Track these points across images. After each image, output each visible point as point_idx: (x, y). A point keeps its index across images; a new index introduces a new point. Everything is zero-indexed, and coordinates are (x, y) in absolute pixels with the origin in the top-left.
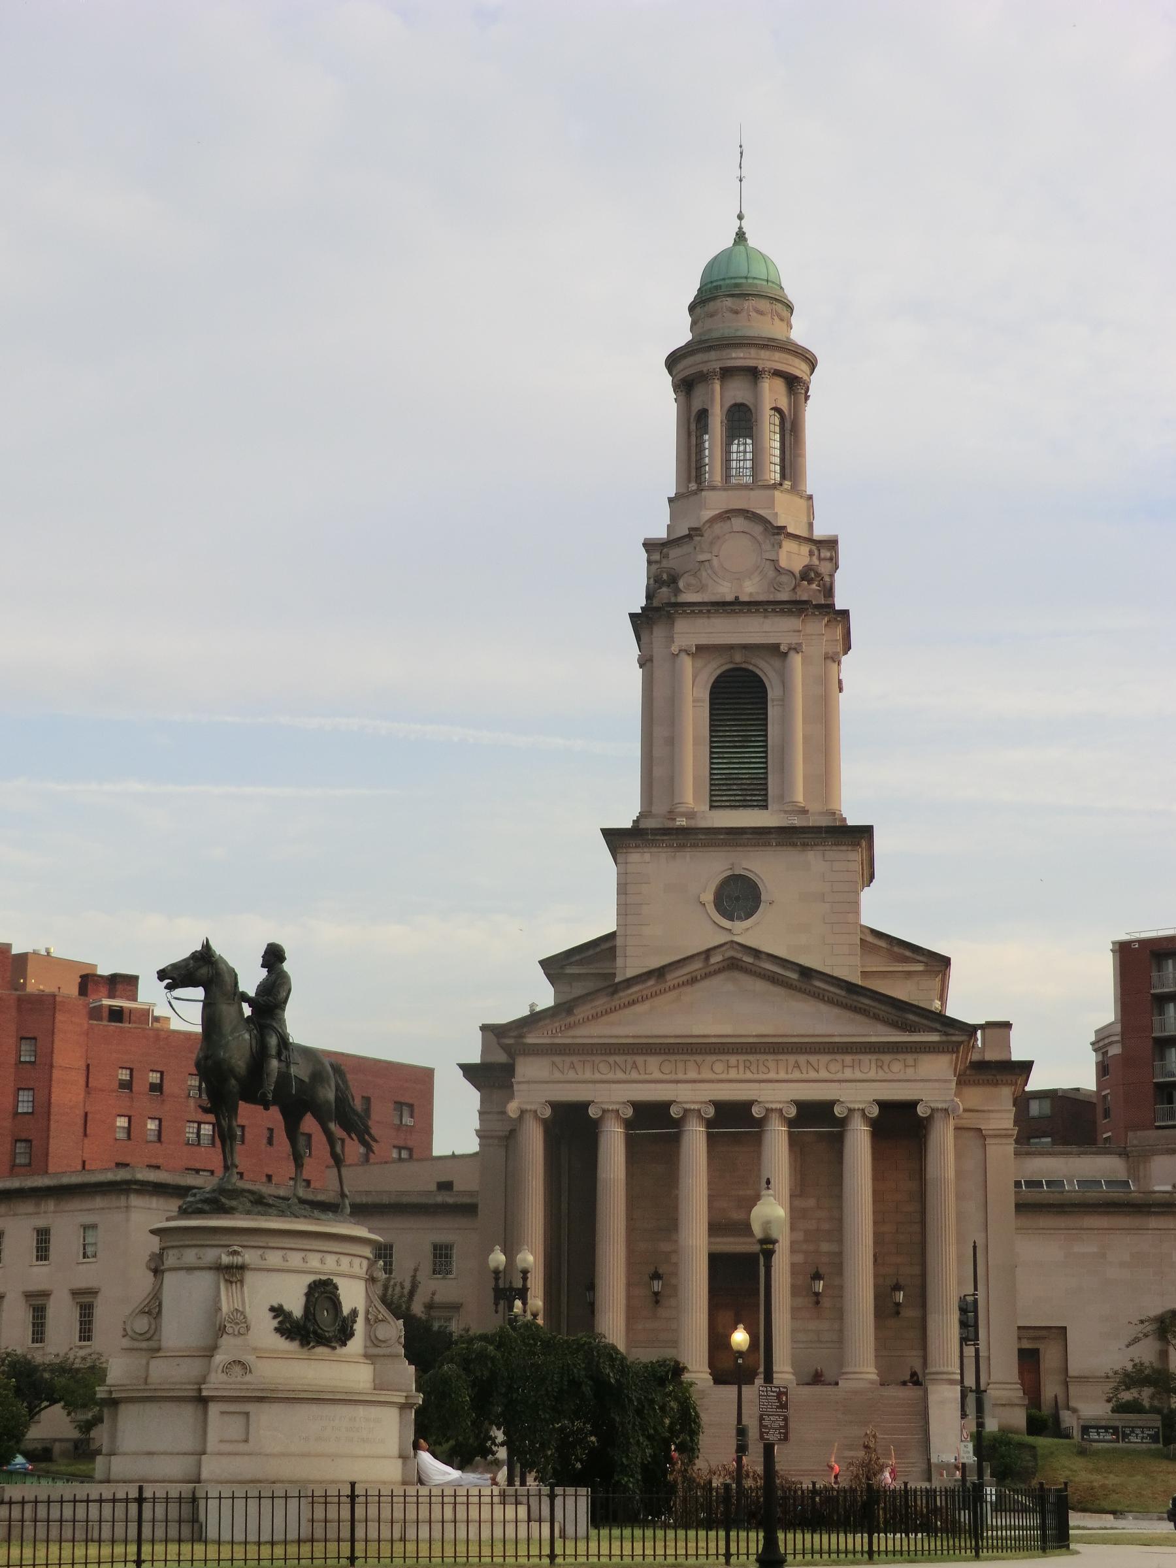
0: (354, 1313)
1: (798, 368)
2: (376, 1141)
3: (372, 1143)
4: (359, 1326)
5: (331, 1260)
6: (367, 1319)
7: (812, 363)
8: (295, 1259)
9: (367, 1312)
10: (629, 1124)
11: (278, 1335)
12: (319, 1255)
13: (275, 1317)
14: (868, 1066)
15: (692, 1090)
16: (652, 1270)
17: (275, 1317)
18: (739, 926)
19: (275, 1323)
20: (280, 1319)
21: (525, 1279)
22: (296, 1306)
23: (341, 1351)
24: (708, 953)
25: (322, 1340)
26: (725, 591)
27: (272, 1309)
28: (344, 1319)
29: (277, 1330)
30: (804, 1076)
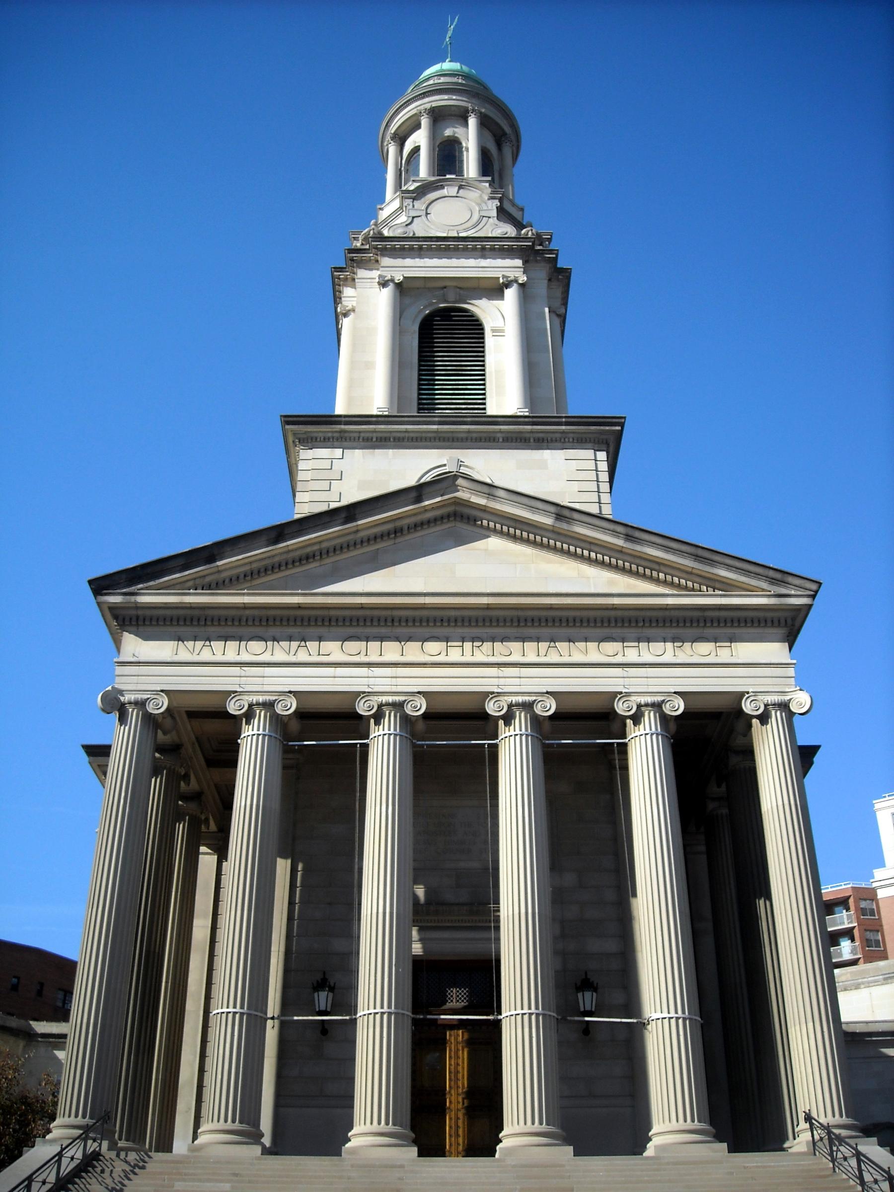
16: (319, 976)
24: (418, 492)
30: (566, 659)
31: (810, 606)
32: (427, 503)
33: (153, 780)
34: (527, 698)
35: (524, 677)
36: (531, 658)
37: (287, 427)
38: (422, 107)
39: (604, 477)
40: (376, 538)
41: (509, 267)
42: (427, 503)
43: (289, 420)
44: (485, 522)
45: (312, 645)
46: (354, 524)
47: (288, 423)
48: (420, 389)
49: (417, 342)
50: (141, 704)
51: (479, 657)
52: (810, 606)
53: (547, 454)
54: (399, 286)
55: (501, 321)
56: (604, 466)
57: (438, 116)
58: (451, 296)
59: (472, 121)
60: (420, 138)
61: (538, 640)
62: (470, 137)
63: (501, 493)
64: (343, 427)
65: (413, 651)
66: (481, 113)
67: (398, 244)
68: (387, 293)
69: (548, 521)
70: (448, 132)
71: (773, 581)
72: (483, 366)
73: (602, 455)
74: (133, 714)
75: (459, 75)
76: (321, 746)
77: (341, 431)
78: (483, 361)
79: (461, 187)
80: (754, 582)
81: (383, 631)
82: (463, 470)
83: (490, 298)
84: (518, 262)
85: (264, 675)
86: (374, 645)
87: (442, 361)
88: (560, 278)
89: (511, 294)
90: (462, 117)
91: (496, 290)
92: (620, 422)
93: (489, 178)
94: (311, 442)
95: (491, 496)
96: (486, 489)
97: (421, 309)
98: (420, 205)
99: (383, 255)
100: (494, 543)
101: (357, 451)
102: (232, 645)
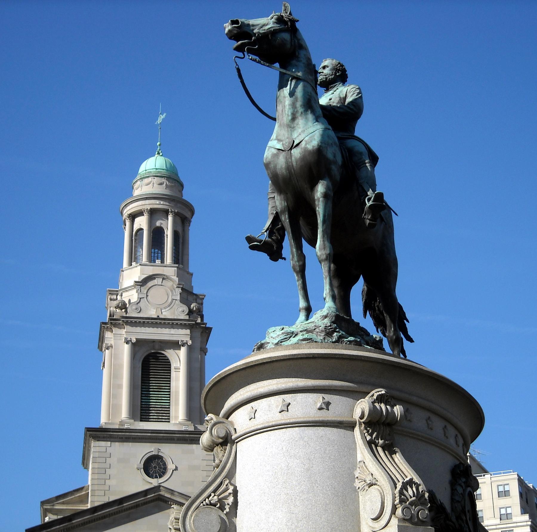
1: (187, 214)
2: (410, 340)
7: (193, 213)
18: (155, 482)
24: (146, 493)
26: (152, 313)
31: (361, 96)
32: (149, 496)
37: (88, 433)
41: (182, 335)
42: (149, 496)
43: (88, 430)
44: (170, 503)
46: (122, 506)
47: (88, 431)
48: (142, 399)
49: (140, 374)
52: (361, 96)
55: (179, 360)
57: (153, 213)
58: (157, 347)
59: (170, 218)
60: (142, 222)
62: (168, 225)
63: (176, 493)
64: (111, 433)
66: (175, 212)
67: (134, 320)
68: (126, 348)
70: (158, 224)
72: (170, 386)
75: (164, 177)
77: (110, 435)
78: (170, 384)
79: (163, 279)
83: (174, 349)
84: (188, 331)
87: (153, 384)
89: (183, 350)
90: (166, 213)
91: (176, 345)
93: (177, 265)
94: (98, 438)
96: (171, 492)
97: (142, 353)
98: (144, 289)
99: (127, 325)
101: (117, 443)
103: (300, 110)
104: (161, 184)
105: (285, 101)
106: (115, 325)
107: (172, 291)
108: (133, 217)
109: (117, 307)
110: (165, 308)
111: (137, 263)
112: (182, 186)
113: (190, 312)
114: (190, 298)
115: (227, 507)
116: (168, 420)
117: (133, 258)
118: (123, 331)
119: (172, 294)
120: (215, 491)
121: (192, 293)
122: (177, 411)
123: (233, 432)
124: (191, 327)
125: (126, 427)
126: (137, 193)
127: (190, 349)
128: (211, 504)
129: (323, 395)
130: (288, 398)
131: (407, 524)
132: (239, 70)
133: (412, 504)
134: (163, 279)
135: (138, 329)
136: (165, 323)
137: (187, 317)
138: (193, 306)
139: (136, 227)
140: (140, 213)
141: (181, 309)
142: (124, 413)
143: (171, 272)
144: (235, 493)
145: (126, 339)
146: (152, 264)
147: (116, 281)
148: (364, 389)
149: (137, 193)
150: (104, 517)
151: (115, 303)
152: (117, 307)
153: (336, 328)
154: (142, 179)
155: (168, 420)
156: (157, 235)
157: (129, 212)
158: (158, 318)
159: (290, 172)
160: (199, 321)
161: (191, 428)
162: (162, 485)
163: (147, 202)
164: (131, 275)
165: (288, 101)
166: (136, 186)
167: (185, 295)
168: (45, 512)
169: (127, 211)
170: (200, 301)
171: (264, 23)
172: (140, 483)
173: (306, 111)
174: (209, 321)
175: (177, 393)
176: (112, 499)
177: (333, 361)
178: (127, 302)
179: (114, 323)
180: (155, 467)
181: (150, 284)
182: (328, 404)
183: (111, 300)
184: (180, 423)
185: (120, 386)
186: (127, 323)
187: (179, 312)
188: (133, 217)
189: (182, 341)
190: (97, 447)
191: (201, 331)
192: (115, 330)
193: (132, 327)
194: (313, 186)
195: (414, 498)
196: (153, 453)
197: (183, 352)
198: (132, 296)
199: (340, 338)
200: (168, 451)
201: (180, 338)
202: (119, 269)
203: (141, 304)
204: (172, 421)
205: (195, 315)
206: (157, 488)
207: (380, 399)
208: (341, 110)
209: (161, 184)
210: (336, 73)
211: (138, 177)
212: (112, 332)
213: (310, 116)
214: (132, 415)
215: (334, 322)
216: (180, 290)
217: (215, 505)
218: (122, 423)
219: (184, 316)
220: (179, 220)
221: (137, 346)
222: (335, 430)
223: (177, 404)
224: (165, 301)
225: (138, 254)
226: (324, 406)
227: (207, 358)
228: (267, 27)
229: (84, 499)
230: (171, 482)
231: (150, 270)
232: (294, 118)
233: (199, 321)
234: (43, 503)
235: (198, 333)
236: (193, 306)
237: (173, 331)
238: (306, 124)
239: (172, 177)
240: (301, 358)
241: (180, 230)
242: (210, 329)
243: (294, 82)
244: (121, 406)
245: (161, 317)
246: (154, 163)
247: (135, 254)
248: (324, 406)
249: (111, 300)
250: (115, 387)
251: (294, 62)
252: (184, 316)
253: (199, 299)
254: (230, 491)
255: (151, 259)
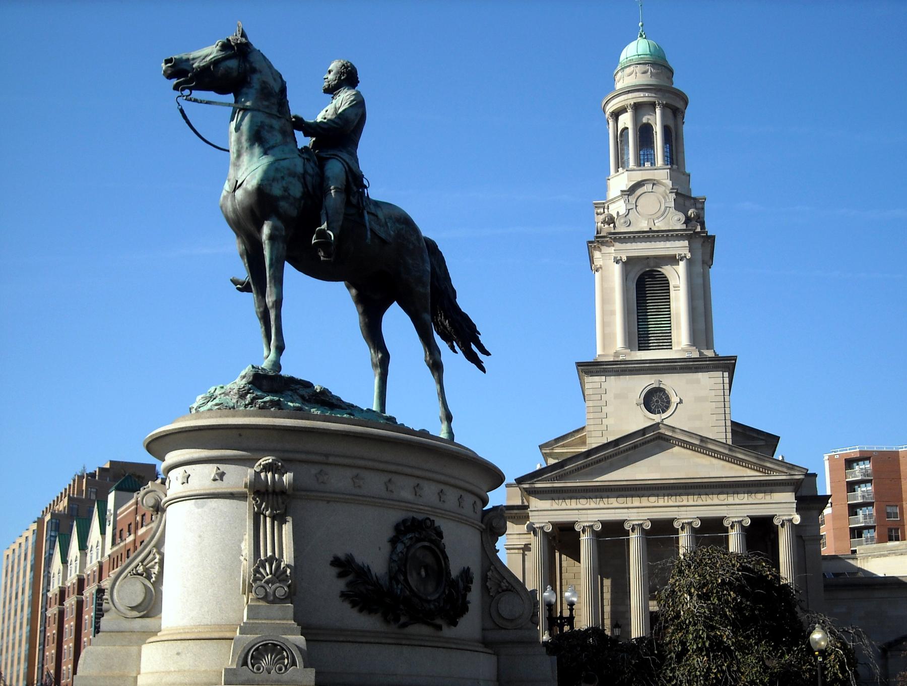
0: (466, 574)
1: (680, 105)
2: (488, 354)
3: (481, 356)
4: (474, 597)
5: (430, 492)
6: (485, 589)
7: (686, 102)
8: (374, 484)
9: (485, 578)
10: (694, 531)
11: (347, 605)
12: (413, 482)
13: (340, 575)
14: (743, 498)
15: (637, 513)
17: (340, 575)
18: (657, 418)
19: (341, 585)
20: (350, 578)
21: (571, 610)
22: (375, 558)
23: (448, 632)
24: (644, 431)
25: (425, 616)
26: (644, 225)
27: (336, 562)
28: (453, 584)
29: (343, 595)
31: (359, 104)
33: (474, 347)
34: (690, 520)
35: (687, 511)
36: (691, 503)
38: (628, 102)
39: (727, 386)
40: (627, 450)
41: (680, 247)
43: (579, 364)
45: (605, 500)
50: (541, 528)
51: (671, 503)
53: (700, 375)
54: (625, 264)
55: (677, 278)
56: (727, 380)
57: (637, 108)
58: (652, 263)
59: (658, 111)
60: (626, 120)
61: (694, 495)
62: (657, 121)
65: (645, 501)
69: (697, 442)
70: (645, 120)
71: (788, 468)
73: (726, 374)
74: (539, 532)
76: (612, 535)
79: (654, 184)
80: (781, 469)
81: (633, 493)
82: (661, 386)
84: (686, 243)
85: (588, 514)
86: (629, 499)
87: (651, 306)
88: (710, 241)
90: (653, 105)
91: (673, 260)
92: (735, 358)
95: (673, 431)
98: (632, 199)
100: (677, 449)
102: (573, 501)
103: (245, 144)
104: (645, 72)
105: (233, 134)
106: (603, 243)
107: (664, 198)
108: (616, 115)
109: (604, 222)
110: (658, 218)
111: (623, 168)
112: (671, 71)
113: (688, 220)
114: (688, 203)
115: (153, 576)
116: (670, 347)
117: (620, 163)
118: (612, 250)
119: (665, 200)
120: (142, 562)
121: (689, 198)
122: (679, 335)
123: (163, 496)
124: (689, 238)
125: (621, 358)
126: (619, 86)
127: (690, 263)
128: (139, 574)
129: (218, 465)
130: (187, 468)
131: (262, 603)
132: (182, 111)
133: (267, 582)
134: (654, 184)
135: (628, 246)
136: (658, 236)
137: (684, 227)
138: (691, 212)
139: (620, 128)
140: (623, 110)
141: (676, 218)
142: (619, 342)
143: (663, 175)
144: (161, 563)
145: (615, 258)
146: (642, 168)
147: (605, 189)
148: (256, 456)
149: (619, 86)
150: (599, 461)
151: (601, 217)
152: (604, 222)
153: (250, 389)
154: (623, 69)
155: (670, 347)
156: (645, 134)
157: (611, 110)
158: (651, 231)
159: (237, 215)
160: (699, 229)
161: (696, 355)
162: (665, 422)
163: (630, 95)
164: (619, 182)
165: (233, 136)
166: (617, 78)
167: (681, 200)
168: (546, 456)
169: (611, 107)
170: (700, 206)
171: (207, 52)
172: (639, 420)
173: (252, 145)
174: (710, 230)
175: (678, 315)
176: (611, 439)
177: (220, 431)
178: (615, 216)
179: (600, 241)
180: (657, 401)
181: (639, 191)
182: (221, 475)
183: (598, 214)
184: (683, 350)
185: (613, 313)
186: (615, 240)
187: (675, 221)
188: (616, 115)
189: (680, 255)
190: (593, 382)
191: (702, 243)
192: (605, 249)
193: (454, 292)
194: (259, 229)
195: (270, 576)
196: (654, 386)
197: (682, 267)
198: (618, 208)
199: (253, 400)
200: (671, 383)
201: (676, 252)
202: (605, 176)
203: (630, 216)
204: (675, 348)
205: (694, 222)
206: (656, 426)
207: (267, 468)
208: (326, 126)
209: (645, 72)
210: (340, 77)
211: (619, 68)
212: (600, 251)
213: (257, 150)
214: (629, 344)
215: (249, 383)
216: (674, 196)
217: (142, 575)
218: (617, 354)
219: (680, 226)
220: (669, 112)
221: (629, 264)
222: (228, 501)
223: (679, 328)
224: (657, 211)
225: (625, 158)
226: (217, 477)
227: (713, 271)
228: (208, 59)
229: (583, 442)
230: (676, 419)
231: (639, 176)
232: (239, 155)
233: (699, 229)
234: (541, 447)
235: (698, 244)
236: (691, 212)
237: (669, 244)
238: (250, 161)
239: (659, 63)
240: (186, 431)
241: (671, 123)
242: (713, 238)
243: (241, 113)
244: (614, 335)
245: (654, 229)
246: (637, 48)
247: (622, 158)
248: (217, 477)
249: (598, 214)
250: (607, 313)
251: (245, 90)
252: (680, 226)
253: (698, 203)
254: (157, 560)
255: (639, 163)
